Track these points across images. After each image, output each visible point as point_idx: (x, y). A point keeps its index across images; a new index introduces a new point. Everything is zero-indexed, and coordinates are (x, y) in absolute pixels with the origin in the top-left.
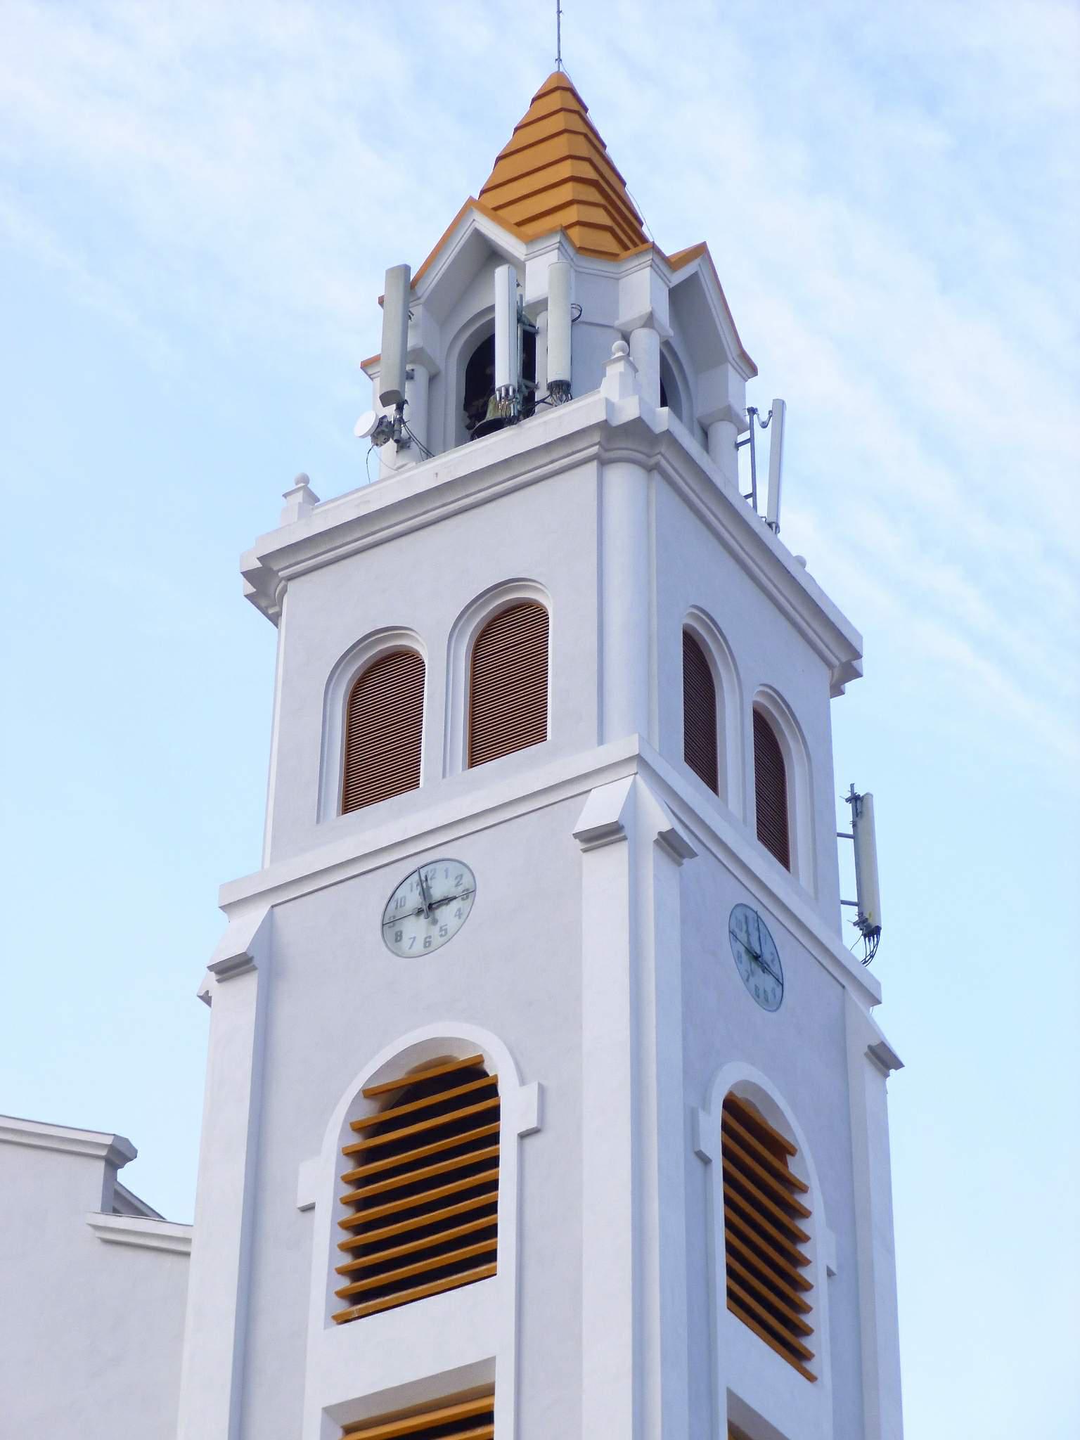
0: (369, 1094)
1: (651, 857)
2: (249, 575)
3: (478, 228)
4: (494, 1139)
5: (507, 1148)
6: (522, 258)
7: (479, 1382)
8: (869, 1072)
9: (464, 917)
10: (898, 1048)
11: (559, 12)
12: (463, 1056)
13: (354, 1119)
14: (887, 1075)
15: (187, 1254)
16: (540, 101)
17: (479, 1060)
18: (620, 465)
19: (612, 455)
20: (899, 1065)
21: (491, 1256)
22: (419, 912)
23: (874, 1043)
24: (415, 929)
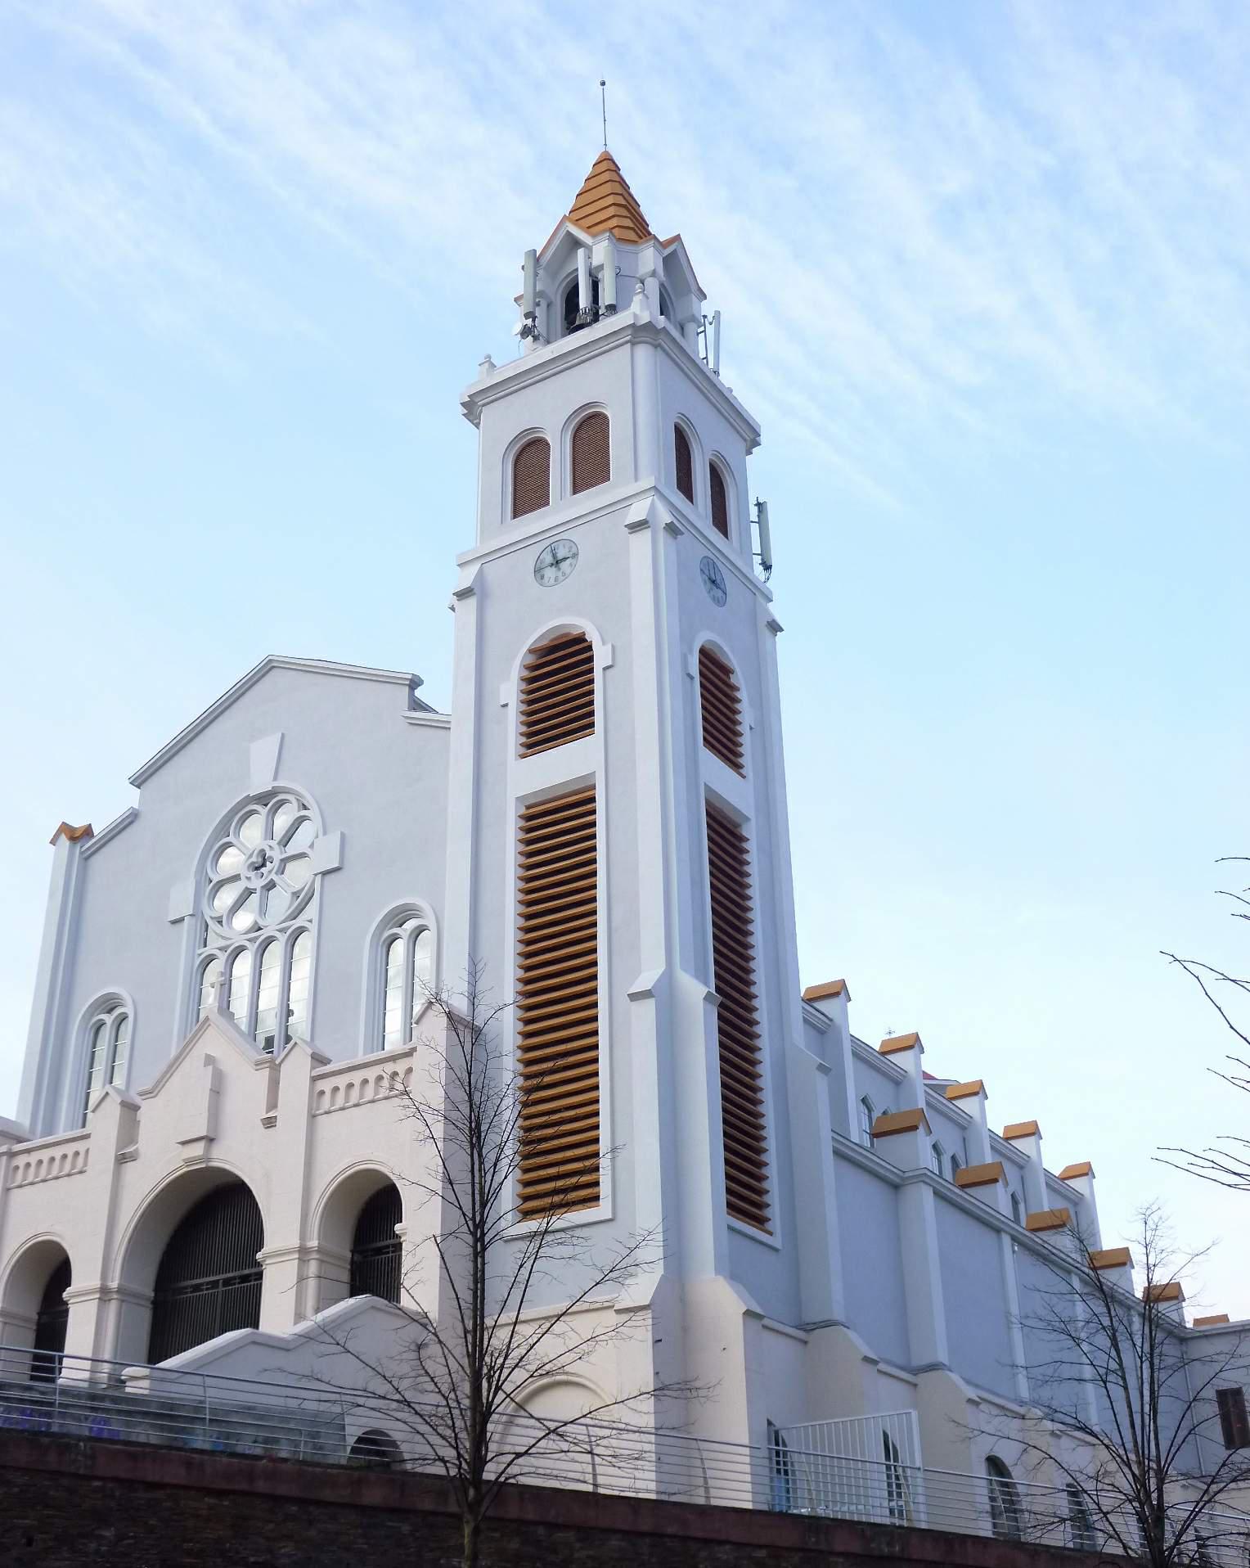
0: (531, 651)
1: (662, 535)
4: (591, 671)
5: (598, 674)
8: (767, 633)
11: (605, 120)
20: (781, 630)
21: (592, 725)
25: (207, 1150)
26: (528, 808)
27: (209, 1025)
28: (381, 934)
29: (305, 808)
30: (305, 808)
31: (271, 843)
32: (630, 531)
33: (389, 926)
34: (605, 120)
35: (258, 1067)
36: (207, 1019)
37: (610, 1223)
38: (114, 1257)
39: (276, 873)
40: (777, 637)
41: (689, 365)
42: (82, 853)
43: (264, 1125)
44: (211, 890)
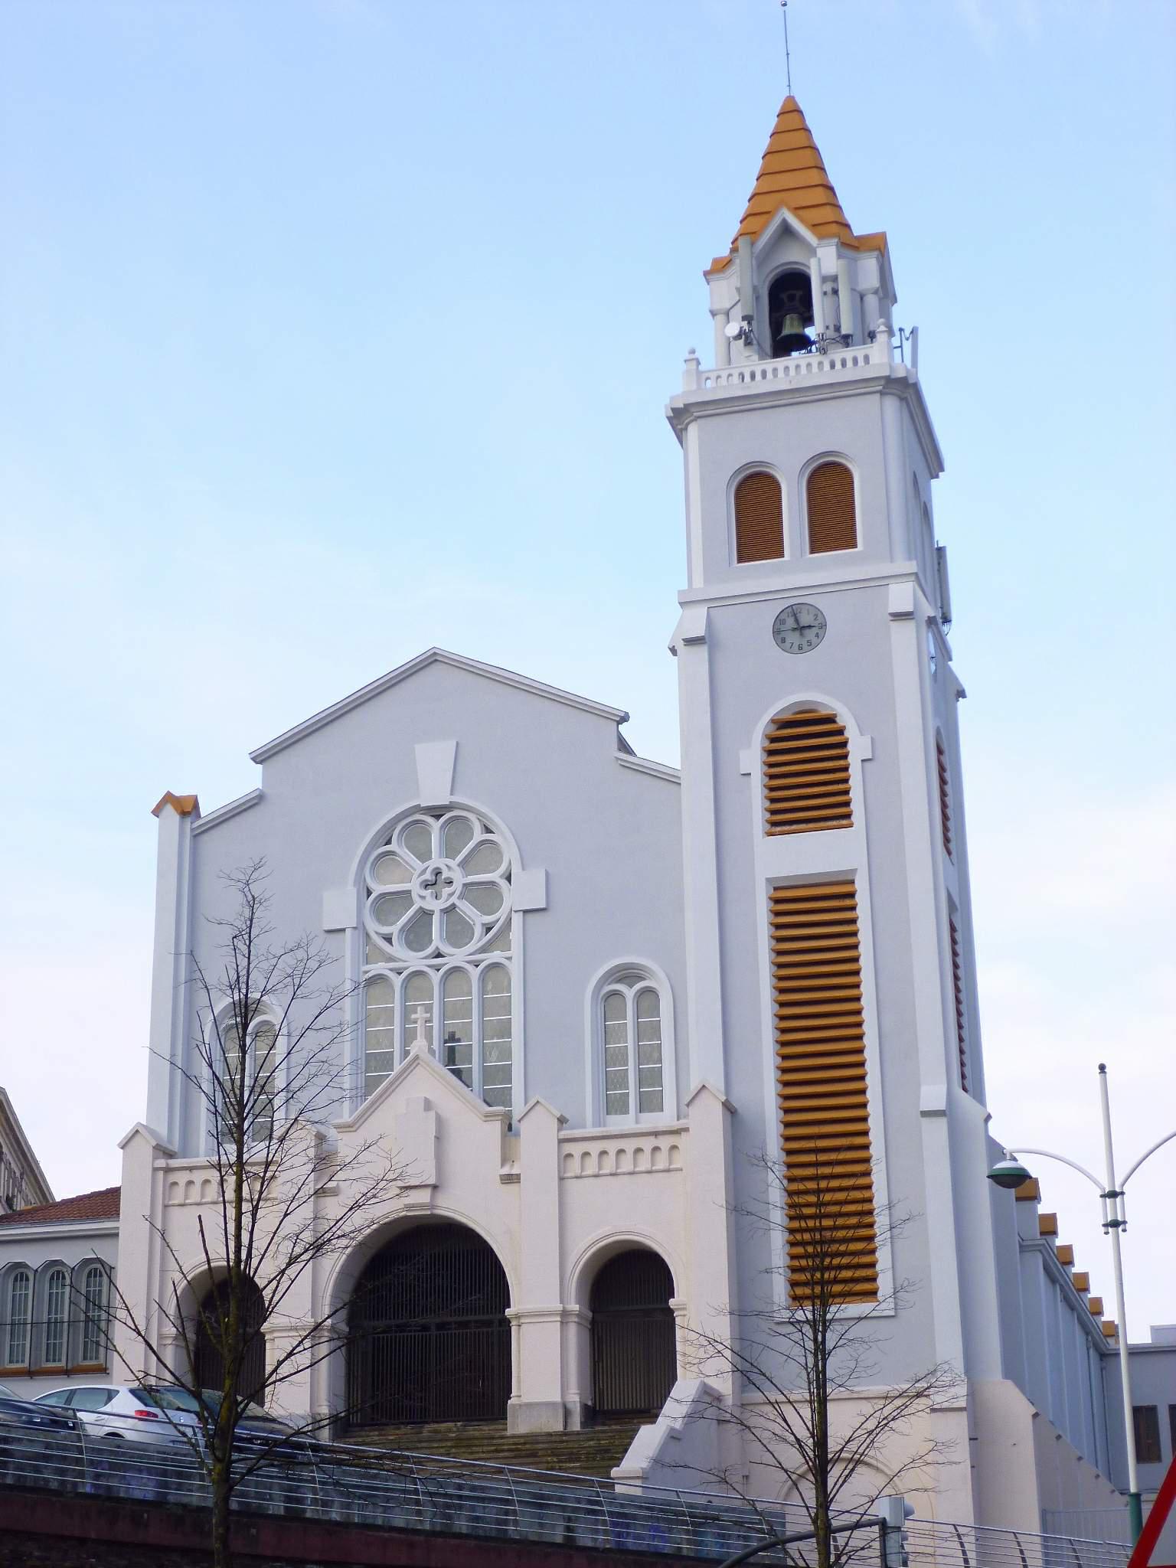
0: (773, 721)
1: (924, 627)
2: (674, 410)
3: (787, 218)
6: (815, 245)
7: (850, 878)
9: (820, 638)
10: (967, 692)
11: (788, 54)
12: (824, 712)
13: (767, 733)
14: (958, 701)
15: (680, 784)
16: (786, 115)
17: (835, 715)
18: (889, 396)
19: (887, 390)
22: (794, 629)
23: (960, 689)
24: (793, 638)
25: (433, 1197)
26: (776, 889)
27: (419, 1064)
28: (600, 990)
29: (488, 831)
30: (488, 831)
31: (449, 861)
32: (892, 619)
33: (610, 980)
34: (788, 54)
35: (488, 1119)
36: (417, 1057)
37: (892, 1320)
38: (321, 1294)
39: (458, 898)
40: (959, 703)
41: (922, 422)
42: (192, 830)
43: (501, 1180)
44: (372, 904)
